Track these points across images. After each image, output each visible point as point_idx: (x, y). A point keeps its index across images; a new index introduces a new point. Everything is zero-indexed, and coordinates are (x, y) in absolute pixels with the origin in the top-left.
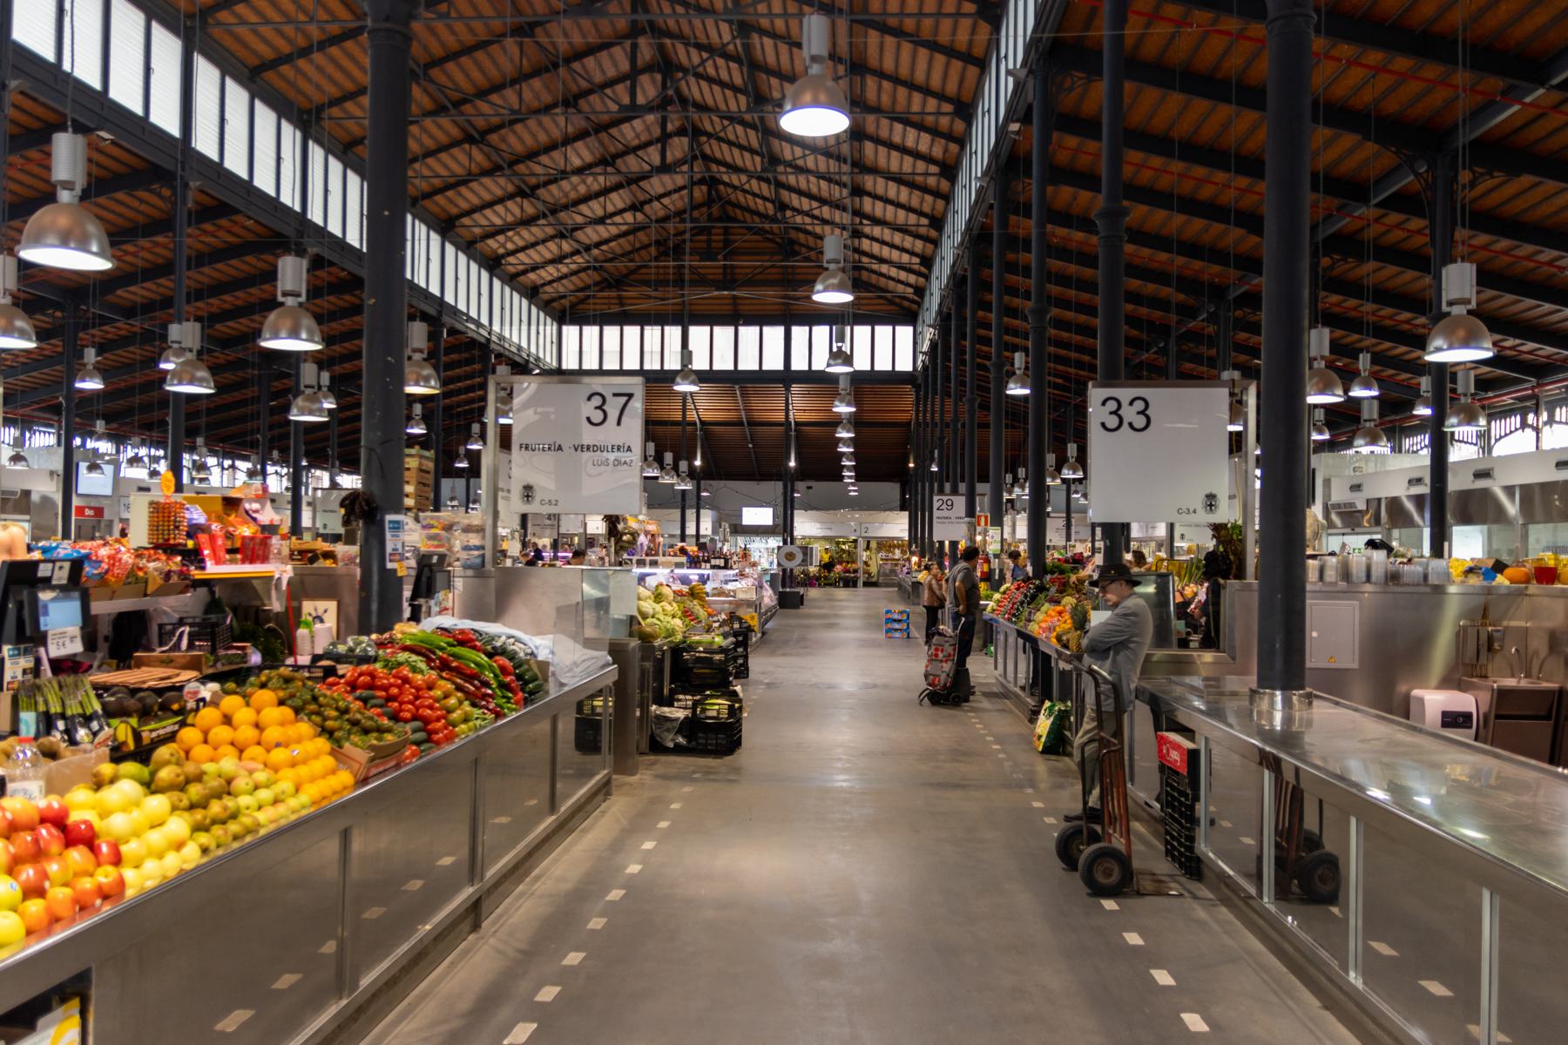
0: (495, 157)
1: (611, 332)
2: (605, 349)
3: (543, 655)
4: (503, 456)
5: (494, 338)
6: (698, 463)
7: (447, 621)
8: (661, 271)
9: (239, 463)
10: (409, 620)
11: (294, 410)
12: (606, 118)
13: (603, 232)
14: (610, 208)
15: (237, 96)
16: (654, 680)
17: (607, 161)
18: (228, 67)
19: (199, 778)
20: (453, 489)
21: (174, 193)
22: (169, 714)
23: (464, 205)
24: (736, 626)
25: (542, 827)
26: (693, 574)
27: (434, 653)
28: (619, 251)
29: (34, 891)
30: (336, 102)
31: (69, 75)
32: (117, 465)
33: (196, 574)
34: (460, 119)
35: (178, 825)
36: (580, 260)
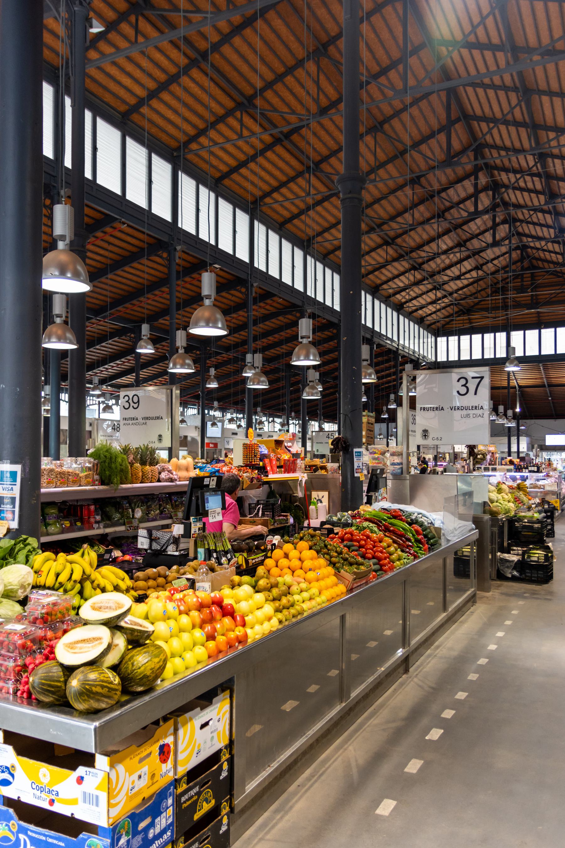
0: (400, 251)
1: (465, 339)
2: (461, 348)
3: (437, 524)
4: (412, 413)
5: (400, 348)
6: (518, 410)
7: (386, 504)
8: (494, 302)
9: (276, 419)
10: (366, 503)
11: (305, 394)
12: (460, 220)
13: (459, 284)
14: (463, 270)
15: (274, 237)
16: (499, 538)
17: (460, 244)
18: (270, 225)
19: (276, 585)
20: (380, 429)
21: (247, 290)
22: (260, 551)
23: (384, 278)
24: (546, 506)
25: (439, 619)
26: (518, 475)
27: (381, 522)
28: (469, 293)
29: (211, 637)
30: (320, 234)
31: (181, 229)
32: (223, 422)
33: (265, 479)
34: (381, 233)
35: (269, 609)
36: (447, 301)
